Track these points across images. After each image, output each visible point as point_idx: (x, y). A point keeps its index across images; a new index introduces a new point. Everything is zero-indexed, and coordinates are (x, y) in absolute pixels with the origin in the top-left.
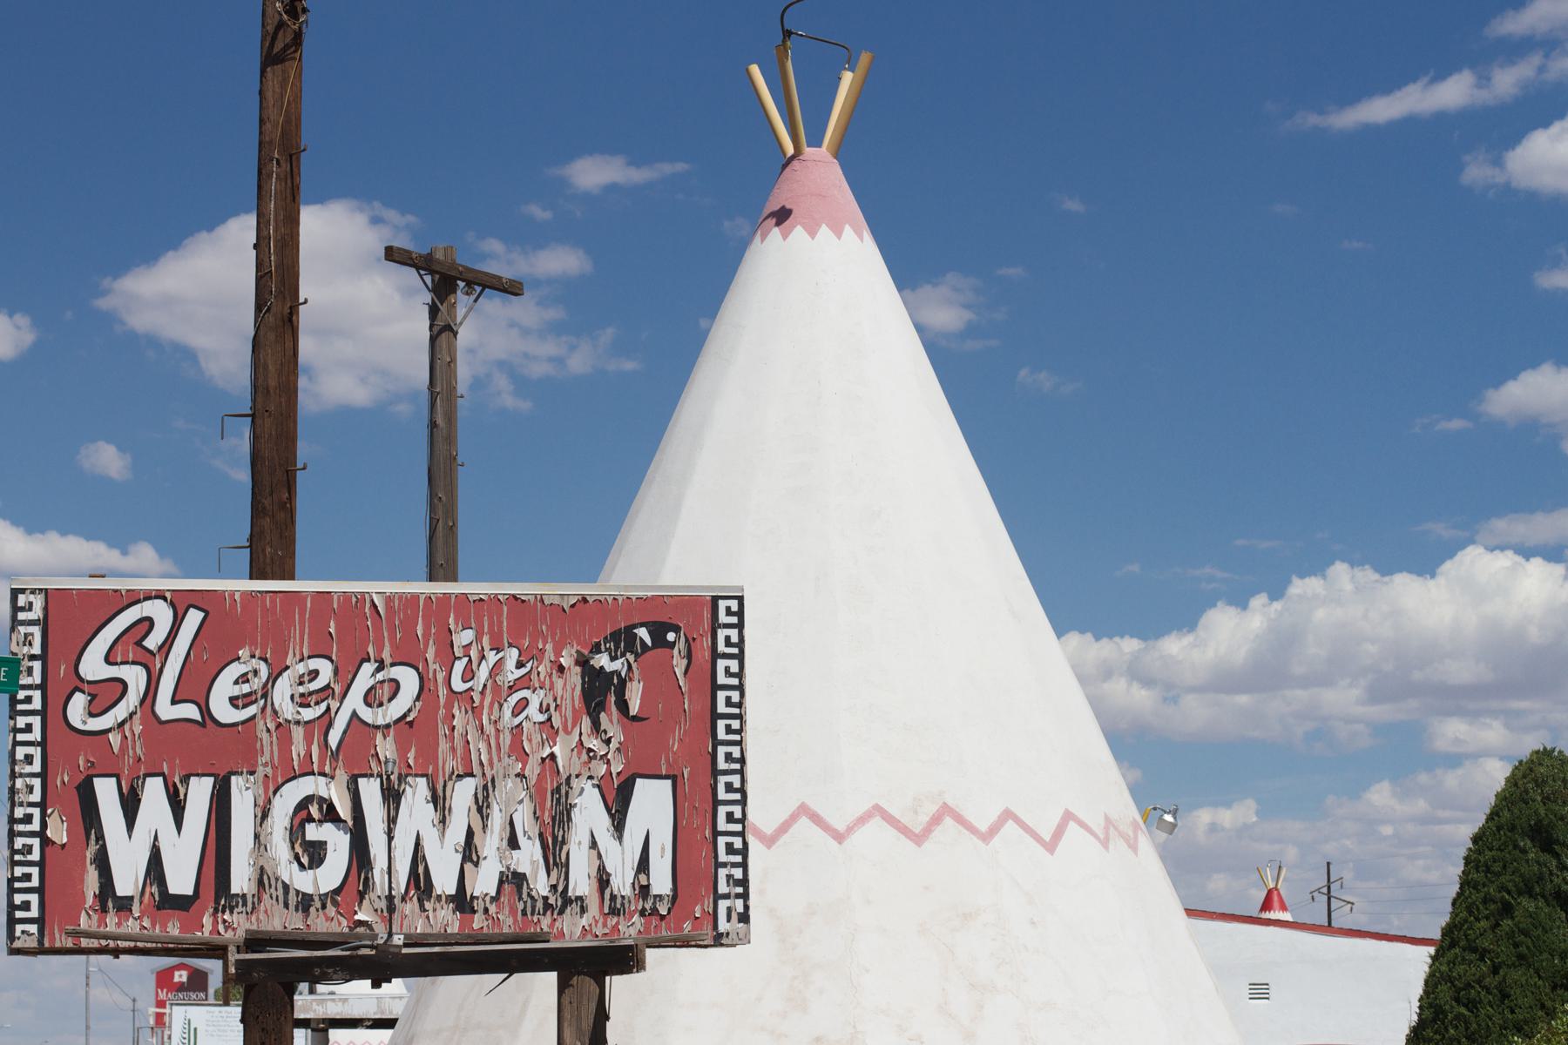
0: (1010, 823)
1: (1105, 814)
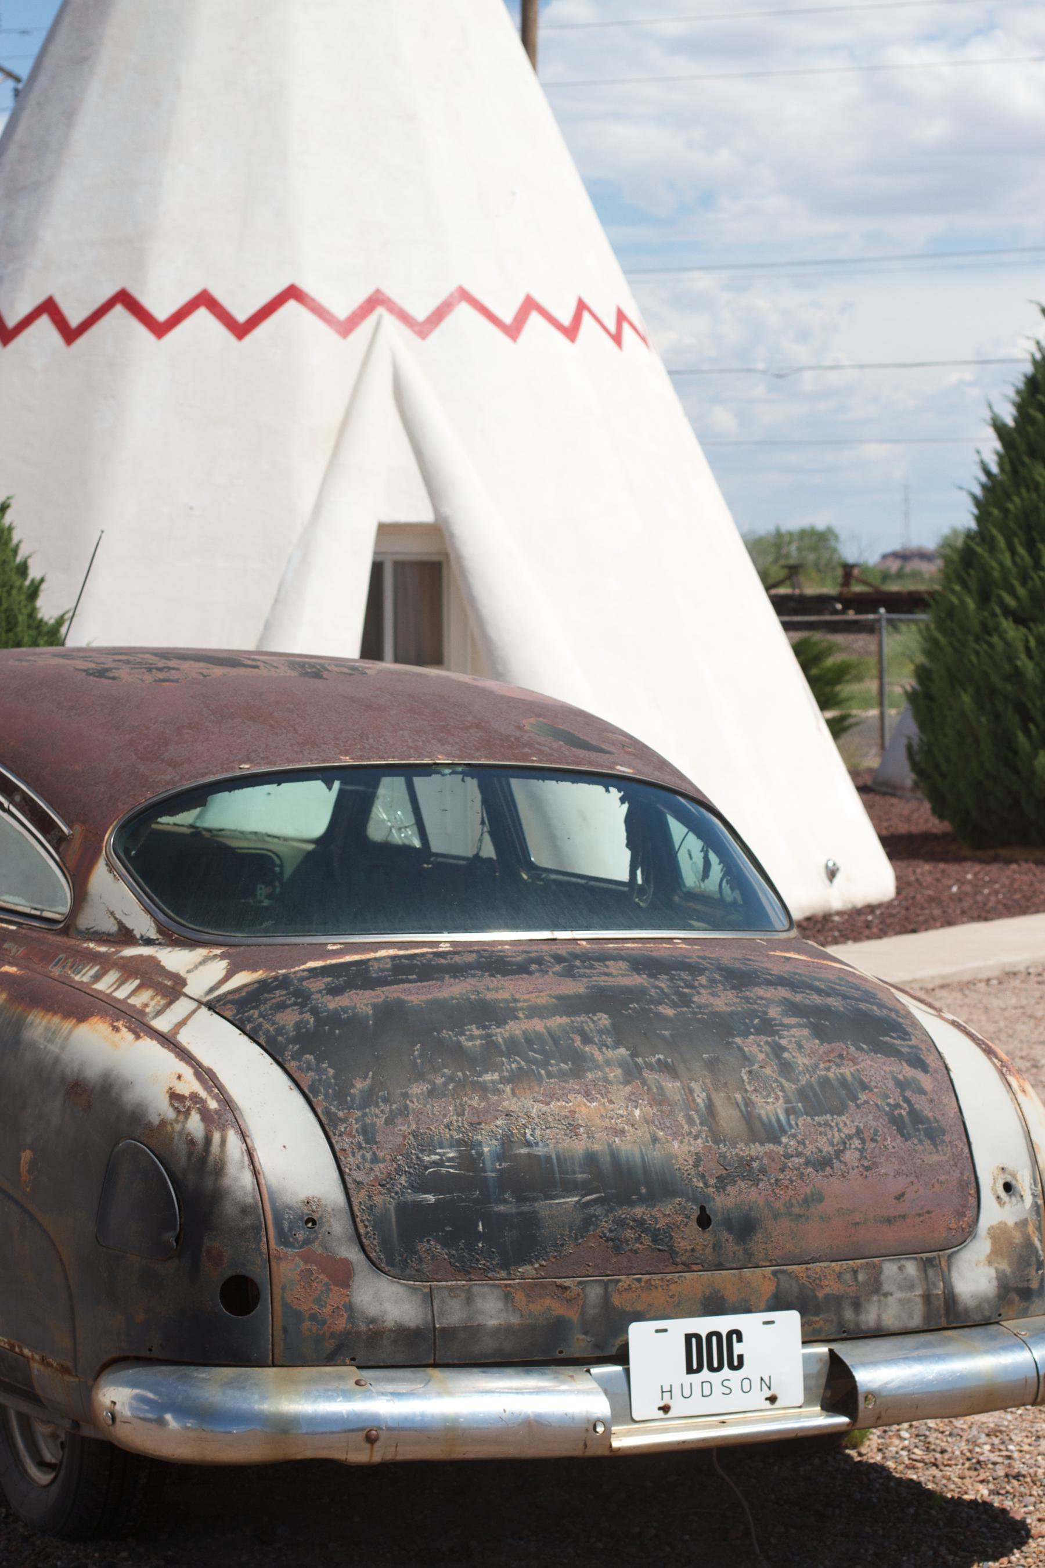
0: (161, 313)
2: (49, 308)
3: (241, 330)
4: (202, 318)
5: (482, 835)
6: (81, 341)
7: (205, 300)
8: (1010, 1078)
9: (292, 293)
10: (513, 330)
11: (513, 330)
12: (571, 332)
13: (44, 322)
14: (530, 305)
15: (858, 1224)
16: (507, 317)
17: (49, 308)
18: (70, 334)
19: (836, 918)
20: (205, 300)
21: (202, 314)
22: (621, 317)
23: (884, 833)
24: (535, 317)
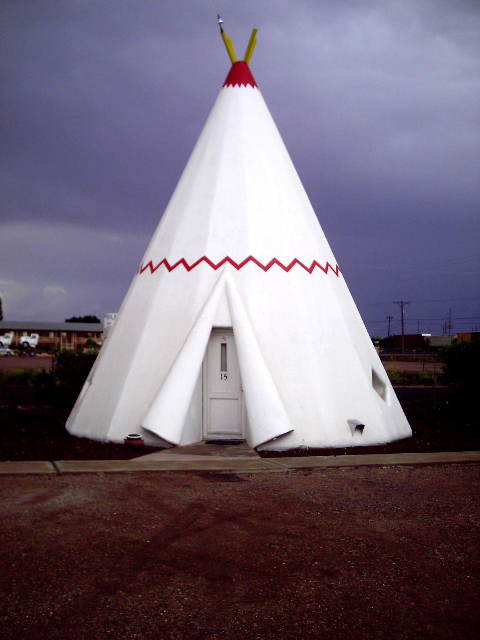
0: (227, 263)
1: (327, 273)
2: (183, 261)
3: (238, 267)
4: (216, 262)
5: (417, 319)
6: (192, 271)
7: (228, 259)
8: (294, 470)
9: (251, 258)
10: (310, 271)
11: (310, 271)
12: (326, 271)
13: (181, 265)
14: (315, 263)
15: (219, 492)
16: (309, 267)
17: (183, 261)
18: (189, 268)
19: (211, 473)
20: (228, 259)
21: (204, 262)
22: (328, 265)
23: (425, 337)
24: (316, 267)
